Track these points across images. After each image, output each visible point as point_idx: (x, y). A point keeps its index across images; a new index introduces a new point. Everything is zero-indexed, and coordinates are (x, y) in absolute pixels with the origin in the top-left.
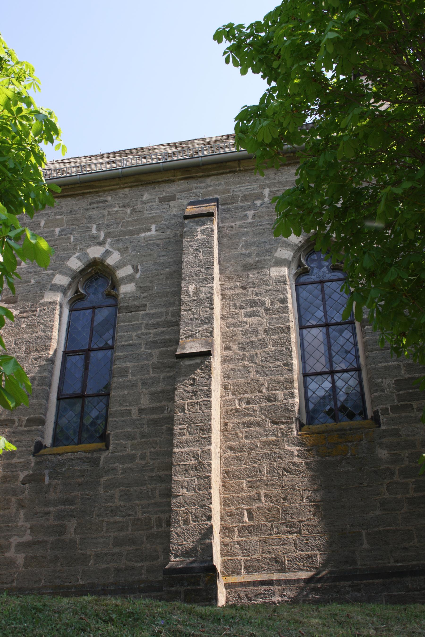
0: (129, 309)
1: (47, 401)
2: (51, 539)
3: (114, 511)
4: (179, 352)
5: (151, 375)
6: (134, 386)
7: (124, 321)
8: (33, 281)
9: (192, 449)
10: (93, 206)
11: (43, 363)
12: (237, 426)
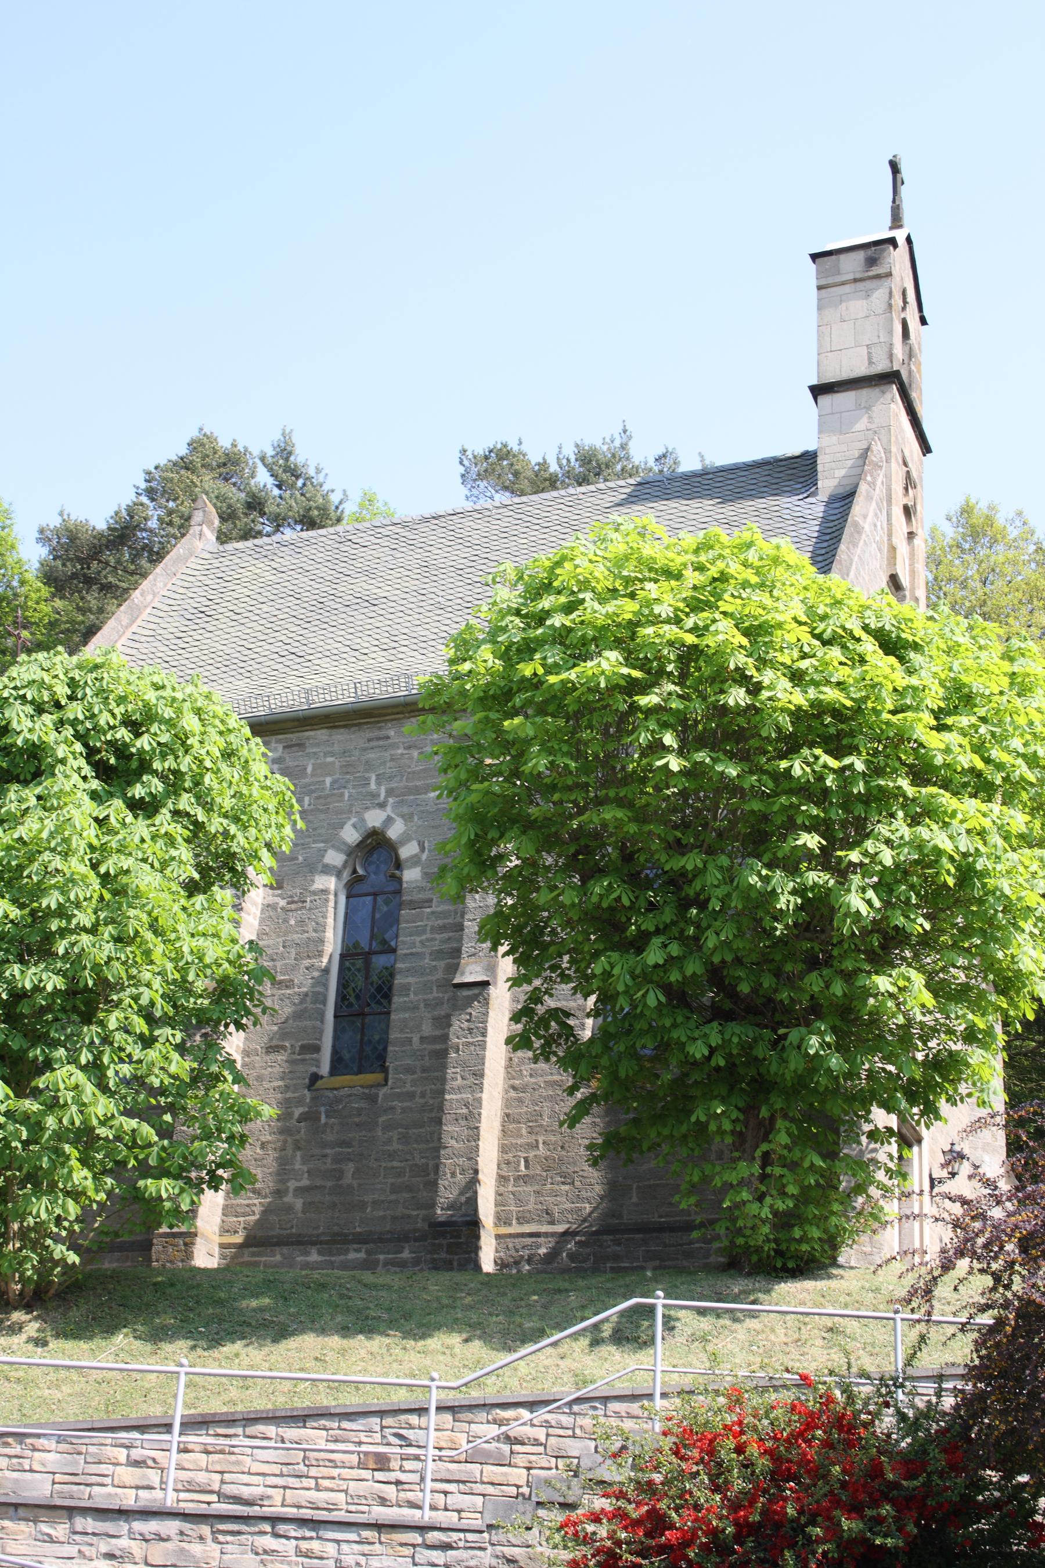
0: (414, 905)
1: (322, 1022)
2: (329, 1184)
3: (392, 1155)
4: (455, 981)
5: (435, 995)
6: (416, 1008)
7: (407, 922)
8: (300, 858)
9: (464, 1096)
10: (372, 744)
11: (316, 974)
12: (522, 1061)
